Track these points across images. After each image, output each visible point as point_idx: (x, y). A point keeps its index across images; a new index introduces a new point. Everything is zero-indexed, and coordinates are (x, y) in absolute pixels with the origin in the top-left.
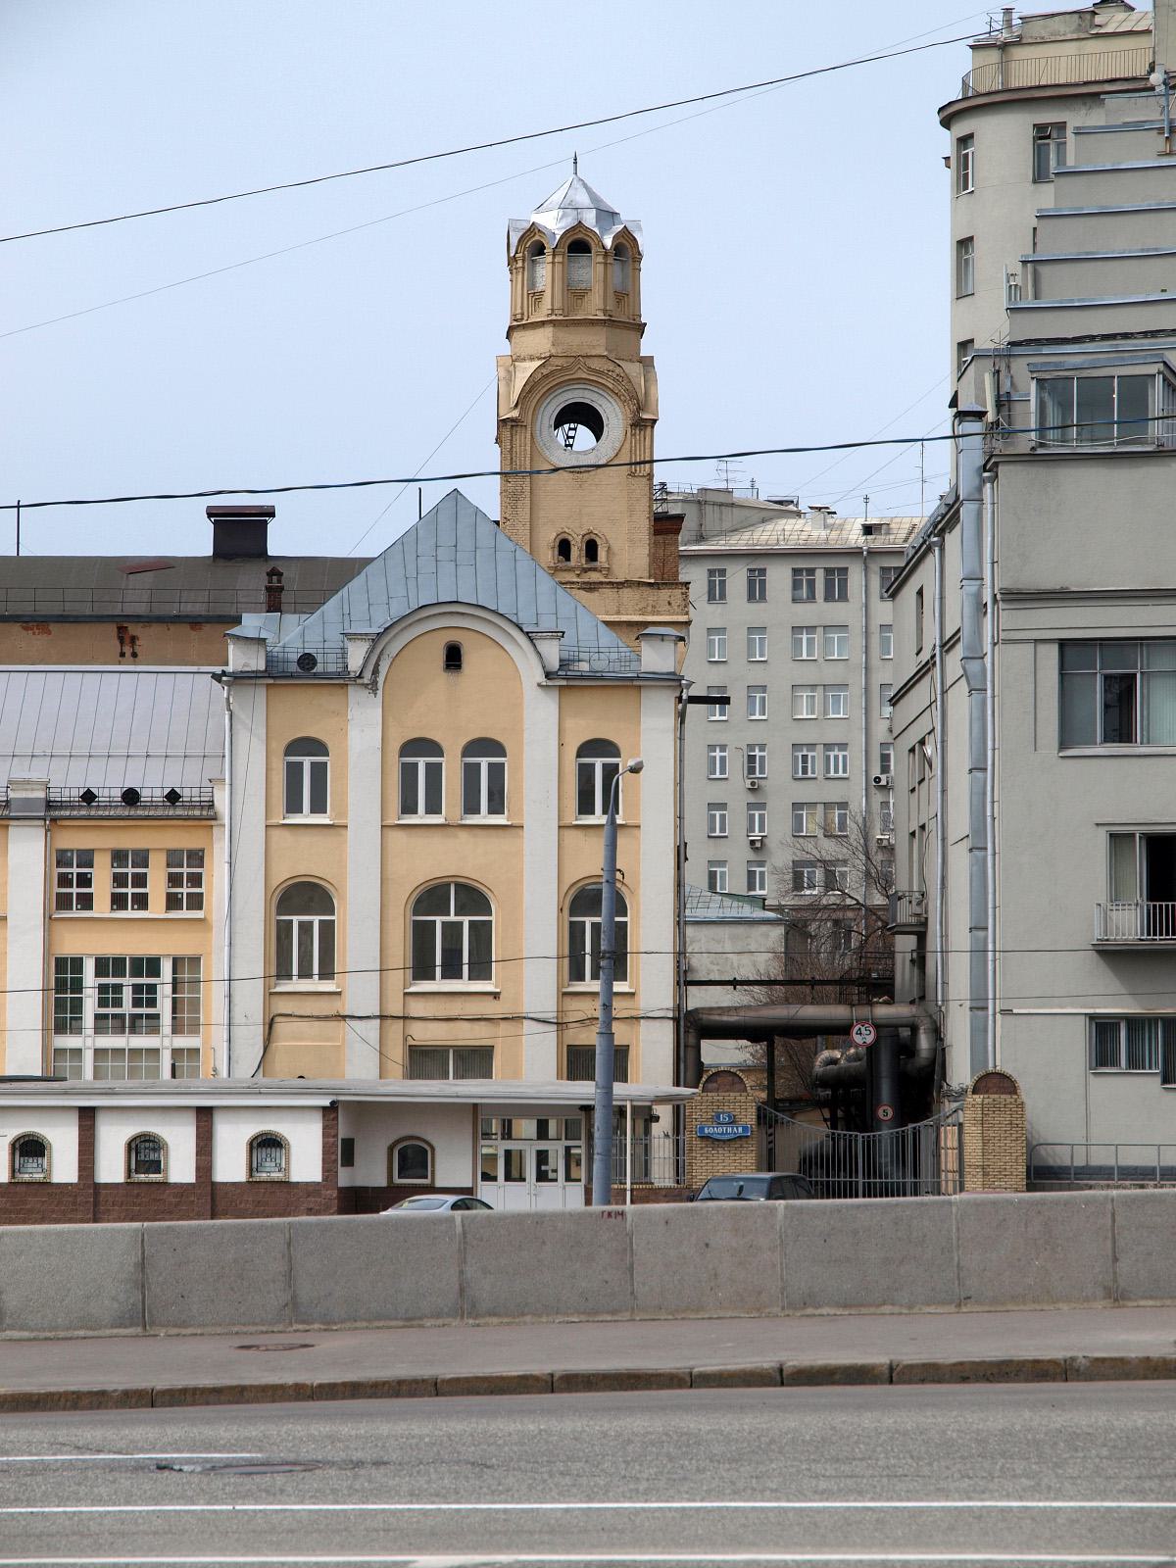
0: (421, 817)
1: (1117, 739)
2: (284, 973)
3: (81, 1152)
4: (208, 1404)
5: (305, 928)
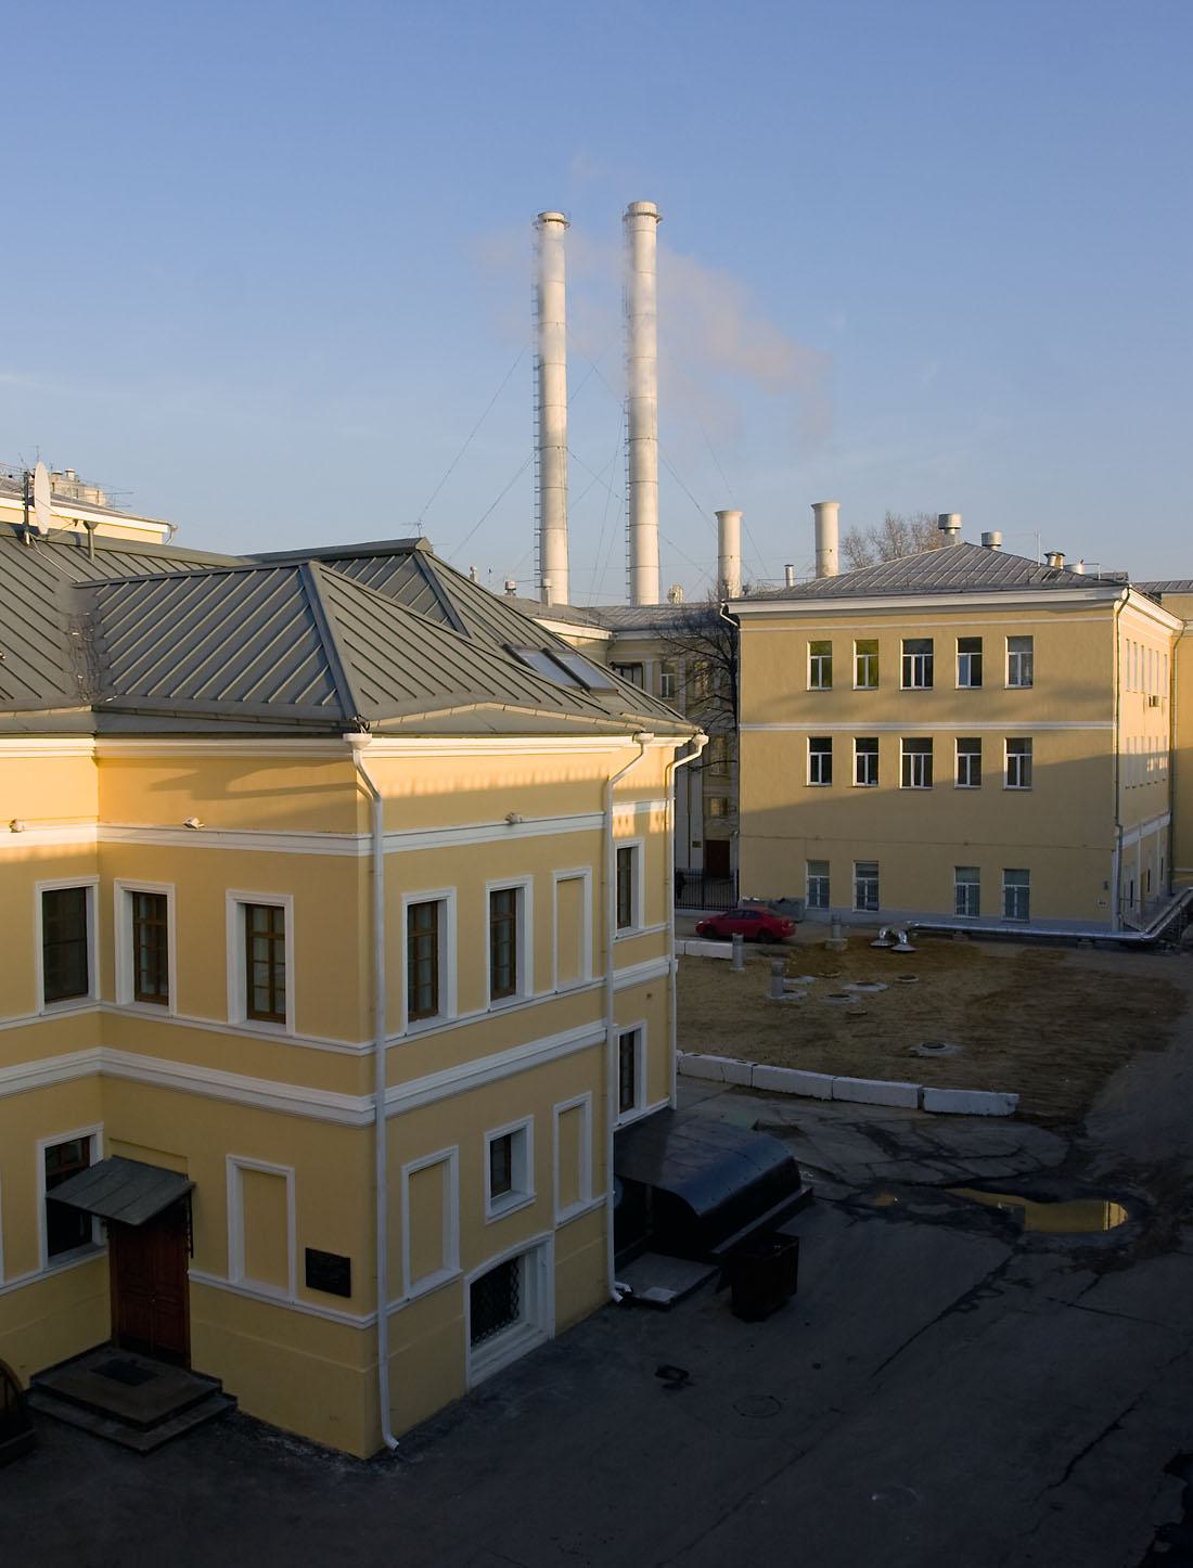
0: (1018, 786)
1: (77, 700)
2: (958, 869)
3: (279, 790)
4: (299, 1440)
5: (918, 759)
